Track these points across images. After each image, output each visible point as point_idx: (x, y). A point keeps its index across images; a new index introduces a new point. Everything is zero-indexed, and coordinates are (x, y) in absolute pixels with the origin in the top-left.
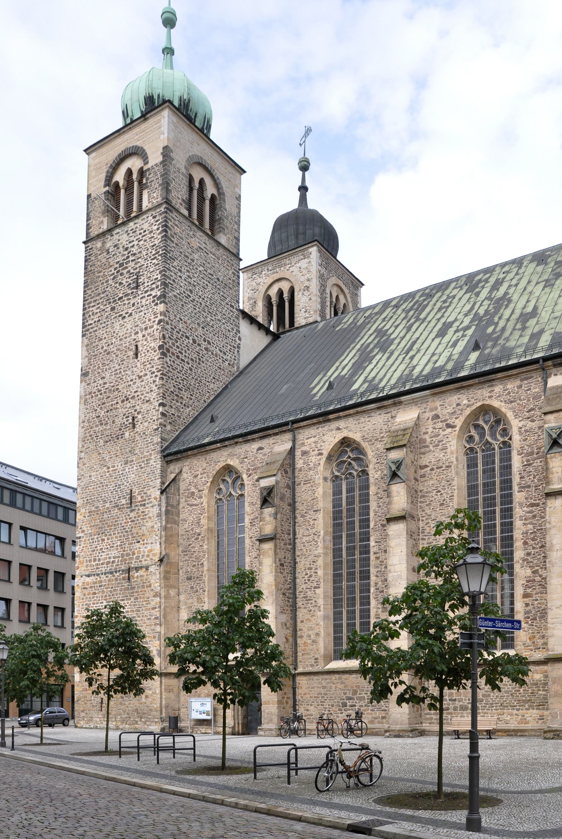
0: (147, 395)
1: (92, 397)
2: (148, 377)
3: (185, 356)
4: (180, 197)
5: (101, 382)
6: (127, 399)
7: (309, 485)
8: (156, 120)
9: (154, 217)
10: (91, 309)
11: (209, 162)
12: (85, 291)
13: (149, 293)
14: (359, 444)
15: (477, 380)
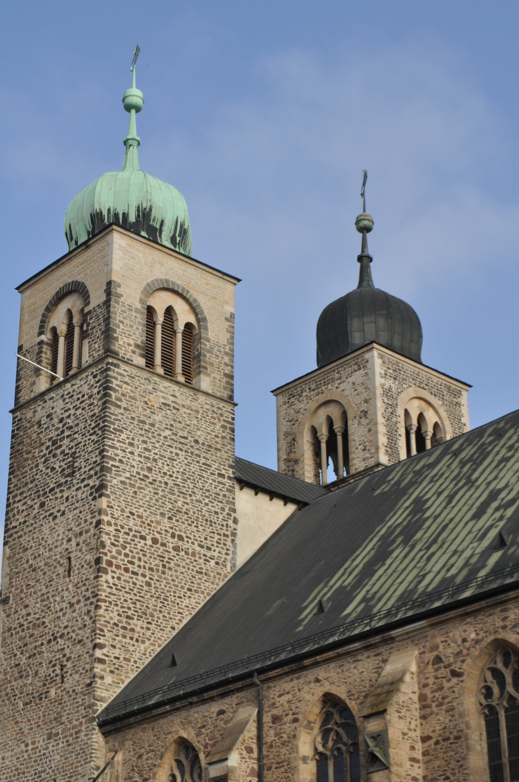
0: (80, 632)
1: (12, 635)
2: (82, 604)
3: (139, 566)
4: (132, 342)
5: (24, 612)
6: (55, 638)
7: (282, 769)
8: (100, 247)
9: (95, 377)
10: (16, 505)
11: (179, 282)
12: (10, 480)
13: (86, 482)
14: (344, 703)
15: (483, 603)
